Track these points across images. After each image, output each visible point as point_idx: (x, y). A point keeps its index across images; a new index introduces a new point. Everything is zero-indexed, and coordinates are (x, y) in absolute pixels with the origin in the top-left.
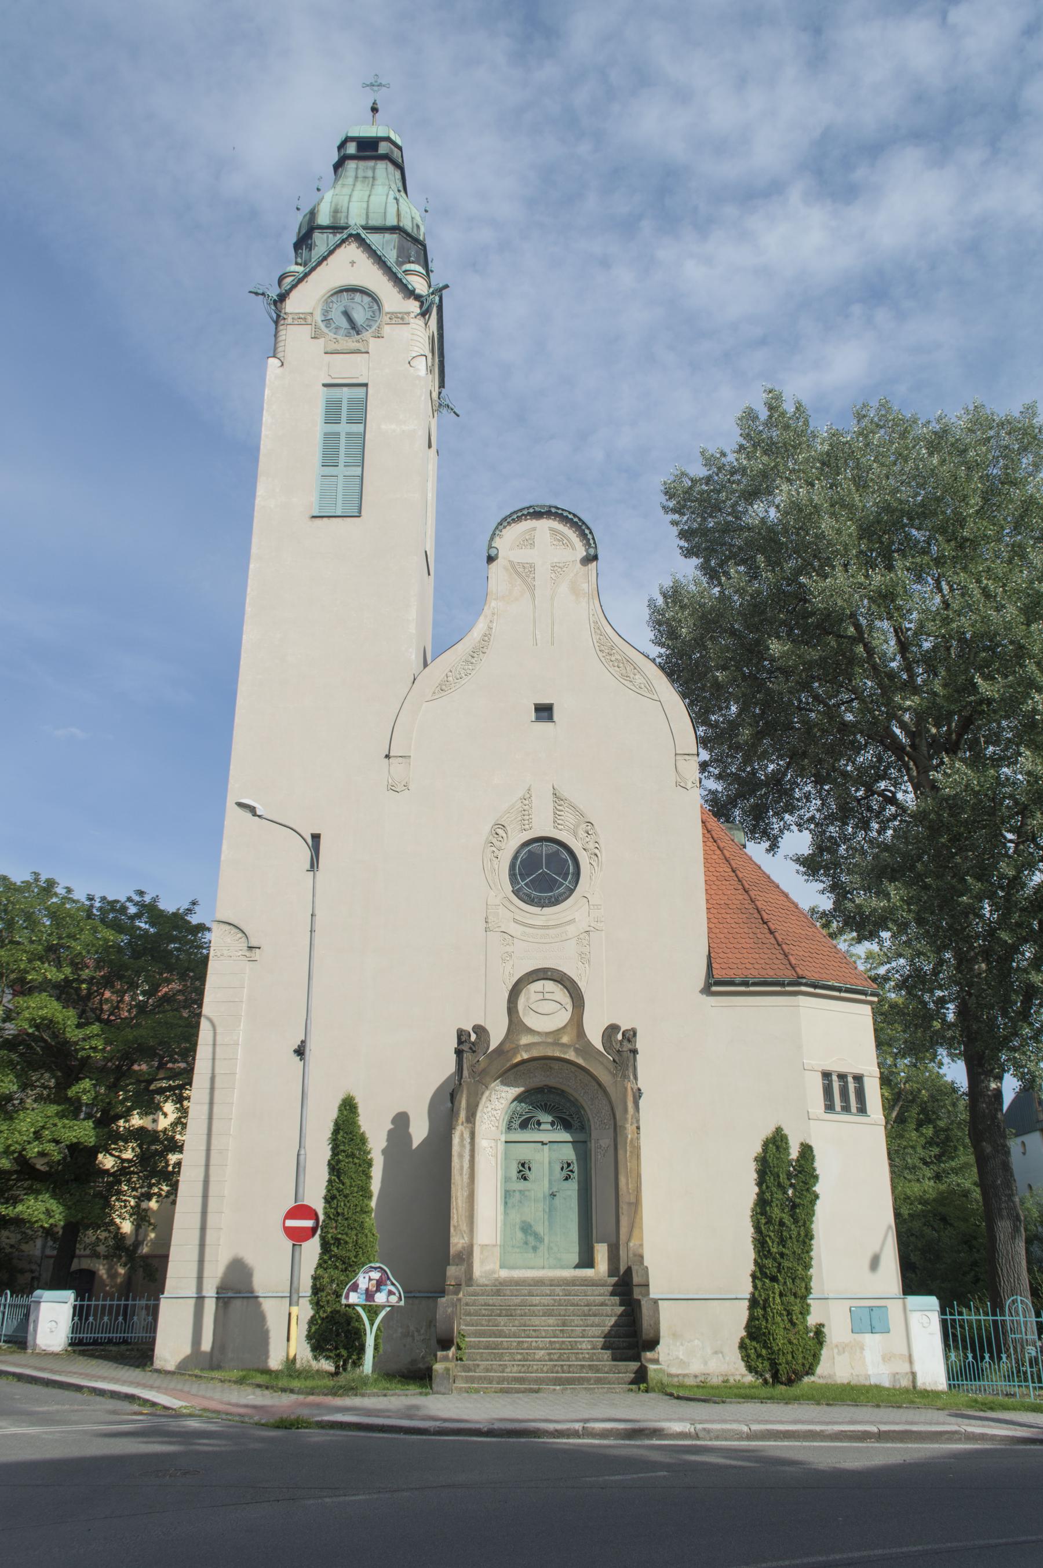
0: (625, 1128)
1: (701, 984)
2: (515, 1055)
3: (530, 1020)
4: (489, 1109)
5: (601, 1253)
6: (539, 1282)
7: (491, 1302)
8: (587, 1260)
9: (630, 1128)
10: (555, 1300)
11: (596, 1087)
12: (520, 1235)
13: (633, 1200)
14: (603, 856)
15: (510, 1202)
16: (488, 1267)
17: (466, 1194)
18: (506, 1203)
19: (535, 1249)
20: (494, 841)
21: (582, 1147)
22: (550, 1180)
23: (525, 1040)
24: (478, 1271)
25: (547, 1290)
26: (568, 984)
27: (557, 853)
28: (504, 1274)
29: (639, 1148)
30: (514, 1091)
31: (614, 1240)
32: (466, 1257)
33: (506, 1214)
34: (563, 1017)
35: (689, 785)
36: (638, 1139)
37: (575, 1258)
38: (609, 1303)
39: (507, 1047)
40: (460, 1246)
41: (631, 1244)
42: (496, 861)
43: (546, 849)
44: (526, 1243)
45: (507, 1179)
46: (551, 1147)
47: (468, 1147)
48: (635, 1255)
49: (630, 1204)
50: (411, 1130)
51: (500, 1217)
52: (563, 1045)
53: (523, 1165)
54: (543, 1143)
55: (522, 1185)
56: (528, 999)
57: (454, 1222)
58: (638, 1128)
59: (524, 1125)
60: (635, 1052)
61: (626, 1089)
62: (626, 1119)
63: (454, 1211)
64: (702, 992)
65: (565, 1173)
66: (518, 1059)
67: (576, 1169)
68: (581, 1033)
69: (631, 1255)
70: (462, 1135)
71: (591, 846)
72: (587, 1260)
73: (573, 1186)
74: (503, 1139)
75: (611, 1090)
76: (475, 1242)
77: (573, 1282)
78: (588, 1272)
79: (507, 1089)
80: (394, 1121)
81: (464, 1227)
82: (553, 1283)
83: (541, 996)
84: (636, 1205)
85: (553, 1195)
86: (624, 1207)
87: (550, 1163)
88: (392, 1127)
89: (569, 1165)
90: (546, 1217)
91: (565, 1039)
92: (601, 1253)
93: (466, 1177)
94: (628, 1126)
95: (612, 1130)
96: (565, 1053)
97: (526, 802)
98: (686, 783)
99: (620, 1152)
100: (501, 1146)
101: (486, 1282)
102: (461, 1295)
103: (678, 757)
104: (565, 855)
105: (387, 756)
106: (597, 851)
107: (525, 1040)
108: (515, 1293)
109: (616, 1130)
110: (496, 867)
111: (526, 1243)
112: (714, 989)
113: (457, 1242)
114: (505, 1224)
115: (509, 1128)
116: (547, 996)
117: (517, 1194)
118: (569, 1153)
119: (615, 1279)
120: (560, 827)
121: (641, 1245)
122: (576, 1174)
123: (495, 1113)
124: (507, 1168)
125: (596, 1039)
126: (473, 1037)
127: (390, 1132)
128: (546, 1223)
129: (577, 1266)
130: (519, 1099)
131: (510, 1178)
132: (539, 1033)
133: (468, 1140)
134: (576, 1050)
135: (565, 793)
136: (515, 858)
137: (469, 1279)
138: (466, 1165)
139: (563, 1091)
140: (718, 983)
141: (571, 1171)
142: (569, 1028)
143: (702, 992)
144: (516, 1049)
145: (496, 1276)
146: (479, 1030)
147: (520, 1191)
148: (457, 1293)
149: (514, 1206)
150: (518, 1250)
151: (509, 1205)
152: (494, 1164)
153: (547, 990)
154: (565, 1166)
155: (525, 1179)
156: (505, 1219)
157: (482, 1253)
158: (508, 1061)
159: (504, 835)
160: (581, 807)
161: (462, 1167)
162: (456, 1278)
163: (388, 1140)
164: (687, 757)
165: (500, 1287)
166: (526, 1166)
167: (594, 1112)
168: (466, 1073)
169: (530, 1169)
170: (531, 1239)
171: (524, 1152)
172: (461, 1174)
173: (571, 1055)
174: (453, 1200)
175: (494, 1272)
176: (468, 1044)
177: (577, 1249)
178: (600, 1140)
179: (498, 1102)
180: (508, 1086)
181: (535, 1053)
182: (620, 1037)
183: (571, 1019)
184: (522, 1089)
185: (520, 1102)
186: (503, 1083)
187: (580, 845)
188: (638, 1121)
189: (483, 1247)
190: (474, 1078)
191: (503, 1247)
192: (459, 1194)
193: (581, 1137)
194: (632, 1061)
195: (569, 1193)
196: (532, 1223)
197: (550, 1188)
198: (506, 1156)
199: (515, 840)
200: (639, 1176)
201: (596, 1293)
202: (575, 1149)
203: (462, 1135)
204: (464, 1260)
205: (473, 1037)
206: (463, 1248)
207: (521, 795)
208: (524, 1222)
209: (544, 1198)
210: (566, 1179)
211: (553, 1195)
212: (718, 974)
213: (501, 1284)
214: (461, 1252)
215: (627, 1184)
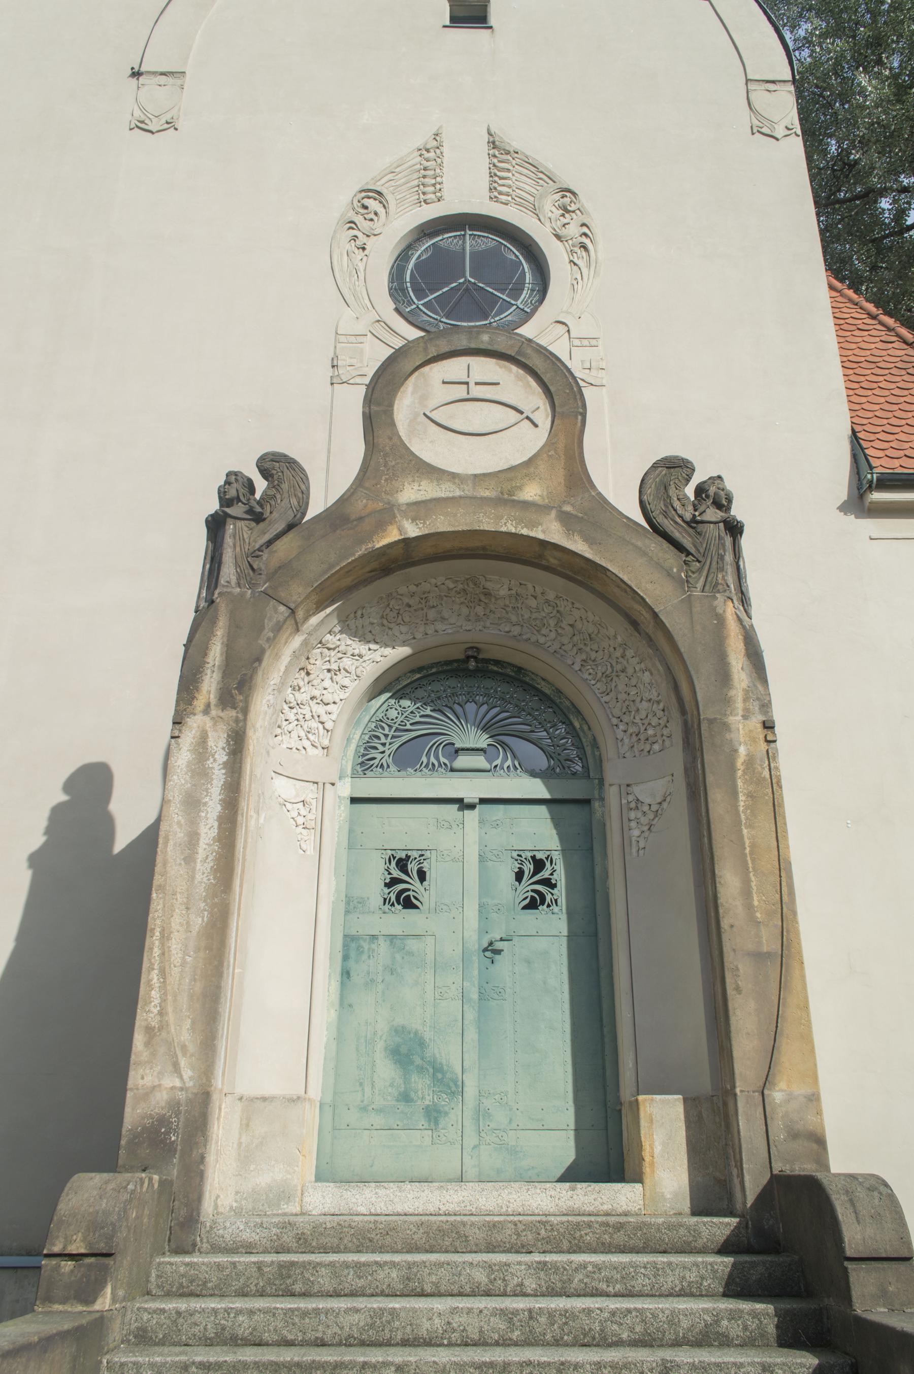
0: (726, 727)
1: (841, 490)
2: (381, 526)
3: (429, 447)
4: (302, 697)
5: (662, 1128)
6: (445, 1235)
7: (244, 1325)
8: (607, 1154)
9: (742, 730)
10: (508, 1315)
11: (617, 629)
12: (386, 1071)
13: (769, 943)
14: (601, 249)
15: (359, 971)
16: (265, 1177)
17: (198, 922)
18: (346, 974)
19: (433, 1115)
20: (359, 219)
21: (577, 809)
22: (482, 907)
23: (411, 492)
24: (230, 1185)
25: (474, 1264)
26: (537, 362)
27: (495, 253)
28: (321, 1201)
29: (775, 784)
30: (382, 657)
31: (705, 1084)
32: (180, 1140)
33: (344, 1004)
34: (528, 441)
35: (780, 132)
36: (770, 757)
37: (564, 1150)
38: (735, 1330)
39: (361, 505)
40: (161, 1099)
41: (777, 1095)
42: (360, 254)
43: (471, 243)
44: (405, 1097)
45: (352, 904)
46: (487, 816)
47: (219, 776)
48: (794, 1135)
49: (759, 957)
50: (114, 807)
51: (325, 1015)
52: (526, 505)
53: (402, 864)
54: (462, 804)
55: (398, 921)
56: (424, 398)
57: (147, 1014)
58: (768, 726)
59: (406, 758)
60: (735, 529)
61: (721, 620)
62: (727, 701)
63: (151, 977)
64: (845, 508)
65: (526, 888)
66: (392, 536)
67: (560, 876)
68: (577, 477)
69: (778, 1133)
70: (203, 740)
71: (573, 230)
72: (607, 1154)
73: (552, 927)
74: (346, 789)
75: (675, 622)
76: (218, 1082)
77: (571, 1236)
78: (620, 1197)
79: (362, 648)
80: (69, 785)
81: (183, 1032)
82: (499, 1236)
83: (461, 391)
84: (782, 959)
85: (492, 950)
86: (741, 972)
87: (482, 859)
88: (64, 798)
89: (539, 865)
90: (471, 1015)
91: (531, 492)
92: (662, 1128)
93: (204, 868)
94: (735, 720)
95: (675, 757)
96: (532, 525)
97: (432, 155)
98: (773, 129)
99: (717, 798)
100: (337, 812)
101: (249, 1236)
102: (104, 1302)
103: (751, 86)
104: (513, 253)
105: (136, 74)
106: (584, 240)
107: (411, 492)
108: (351, 1280)
109: (694, 738)
110: (361, 267)
111: (405, 1097)
112: (878, 496)
113: (153, 1083)
114: (340, 1037)
115: (365, 764)
116: (477, 391)
117: (383, 947)
118: (539, 833)
119: (722, 1226)
120: (503, 198)
121: (814, 1099)
122: (561, 892)
123: (320, 710)
124: (353, 872)
125: (618, 484)
126: (261, 485)
127: (57, 812)
128: (472, 1034)
129: (571, 1175)
130: (393, 684)
131: (362, 901)
132: (453, 476)
133: (222, 757)
134: (566, 519)
135: (515, 139)
136: (403, 257)
137: (181, 1222)
138: (209, 830)
139: (519, 669)
140: (888, 482)
141: (547, 882)
142: (542, 467)
143: (845, 508)
144: (387, 515)
145: (294, 1208)
146: (275, 466)
147: (392, 938)
148: (87, 1292)
149: (370, 983)
150: (378, 1120)
151: (357, 978)
152: (311, 851)
153: (476, 376)
154: (528, 868)
155: (408, 904)
156: (340, 1020)
157: (246, 1125)
158: (361, 541)
159: (381, 210)
160: (550, 166)
161: (193, 838)
162: (94, 1225)
163: (48, 831)
164: (771, 87)
165: (295, 1259)
166: (413, 867)
167: (619, 703)
168: (228, 572)
169: (422, 876)
170: (421, 1084)
171: (407, 829)
172: (189, 860)
173: (551, 531)
174: (154, 942)
175: (284, 1193)
176: (252, 516)
177: (568, 1117)
178: (639, 782)
179: (326, 686)
180: (364, 639)
181: (442, 524)
182: (690, 491)
183: (550, 443)
184: (403, 651)
185: (399, 695)
186: (352, 625)
187: (548, 230)
188: (766, 706)
189: (254, 1104)
190: (252, 586)
191: (331, 1108)
192: (176, 921)
193: (574, 789)
194: (729, 558)
195: (541, 944)
196: (428, 1035)
197: (483, 931)
198: (353, 841)
199: (403, 219)
200: (783, 867)
201: (670, 1281)
202: (557, 822)
203: (203, 740)
204: (170, 1149)
205: (261, 485)
206: (174, 1105)
207: (419, 143)
208: (399, 1031)
209: (465, 958)
210: (532, 905)
211: (492, 950)
212: (882, 465)
213: (304, 1243)
214: (162, 1120)
215: (747, 893)
